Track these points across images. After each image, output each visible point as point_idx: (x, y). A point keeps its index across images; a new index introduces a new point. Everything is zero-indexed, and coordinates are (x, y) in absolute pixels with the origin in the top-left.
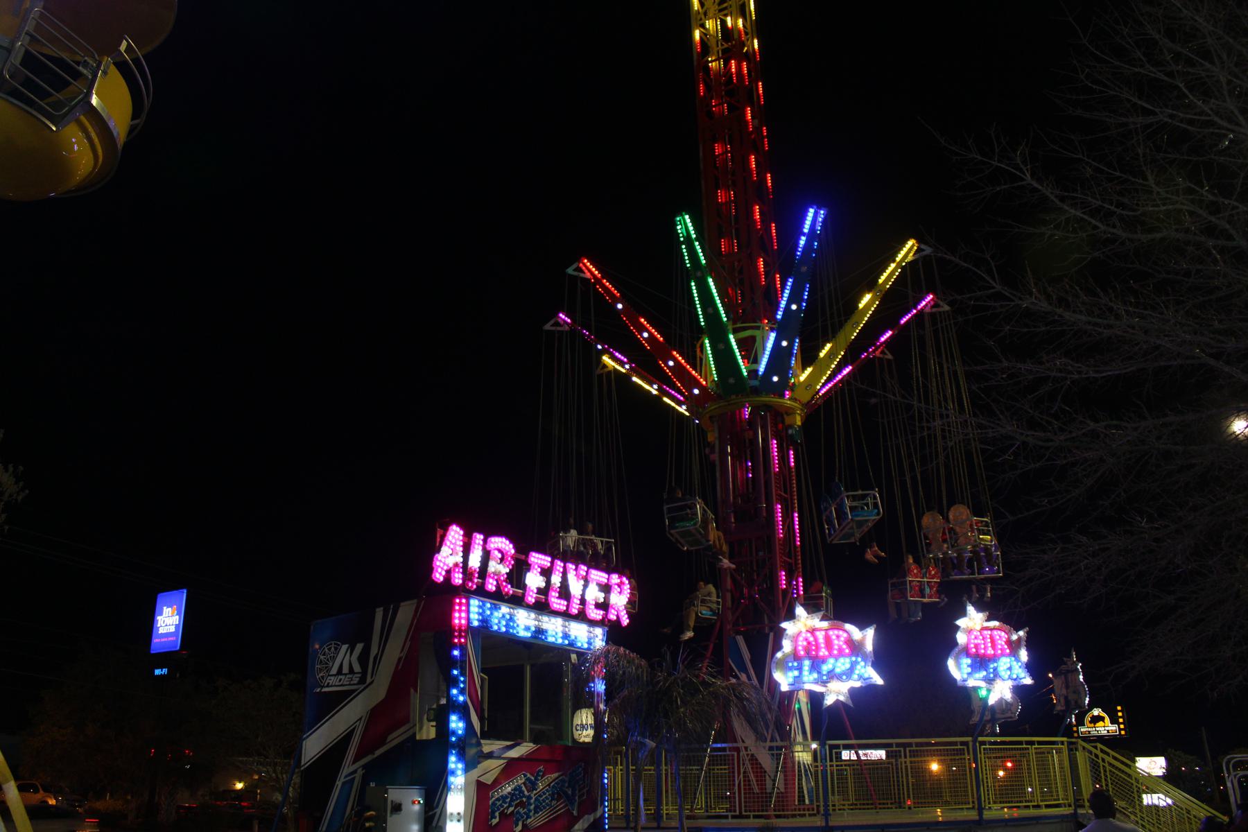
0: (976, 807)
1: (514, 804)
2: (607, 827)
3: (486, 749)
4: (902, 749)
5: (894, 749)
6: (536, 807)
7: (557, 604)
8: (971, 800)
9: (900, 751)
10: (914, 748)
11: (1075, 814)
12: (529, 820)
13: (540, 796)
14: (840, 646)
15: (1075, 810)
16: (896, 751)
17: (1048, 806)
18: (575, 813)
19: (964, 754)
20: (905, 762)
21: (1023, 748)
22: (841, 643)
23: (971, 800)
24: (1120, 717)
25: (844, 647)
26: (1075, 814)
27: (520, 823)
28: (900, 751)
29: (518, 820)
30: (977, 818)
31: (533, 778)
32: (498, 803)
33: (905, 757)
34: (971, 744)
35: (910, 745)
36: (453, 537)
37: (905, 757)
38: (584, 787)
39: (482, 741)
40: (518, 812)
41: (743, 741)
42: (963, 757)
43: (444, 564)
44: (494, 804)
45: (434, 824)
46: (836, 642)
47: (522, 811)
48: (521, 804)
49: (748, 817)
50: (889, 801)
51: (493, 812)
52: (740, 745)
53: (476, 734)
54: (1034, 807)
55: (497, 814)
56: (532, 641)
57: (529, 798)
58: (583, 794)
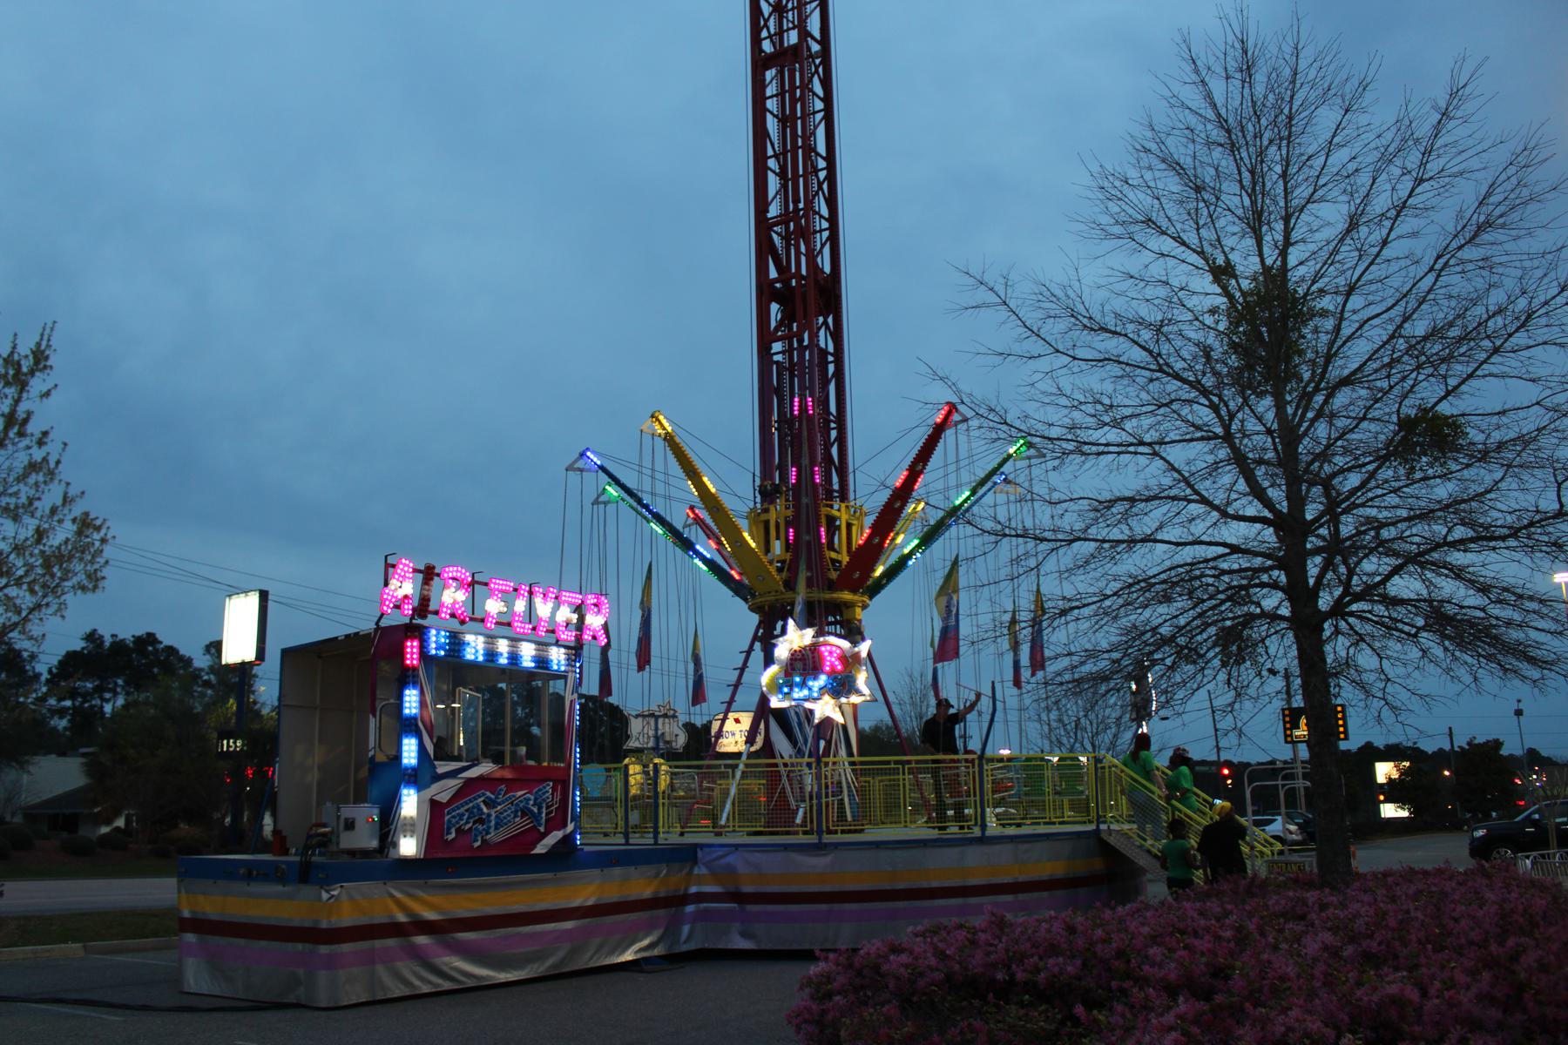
0: (979, 823)
1: (472, 821)
2: (578, 842)
3: (440, 770)
4: (730, 770)
5: (893, 766)
6: (497, 824)
7: (520, 628)
8: (903, 820)
9: (898, 769)
10: (913, 765)
11: (1098, 830)
12: (489, 837)
13: (501, 813)
14: (832, 663)
15: (1098, 826)
16: (894, 769)
17: (843, 832)
18: (542, 829)
19: (898, 774)
20: (904, 779)
21: (890, 769)
22: (829, 658)
23: (903, 820)
24: (1341, 726)
25: (837, 663)
26: (1098, 830)
27: (479, 838)
28: (898, 769)
29: (476, 836)
30: (817, 841)
31: (493, 796)
32: (454, 821)
33: (904, 774)
34: (977, 762)
35: (909, 762)
36: (402, 570)
37: (904, 774)
38: (552, 805)
39: (436, 763)
40: (476, 829)
41: (782, 757)
42: (896, 777)
43: (393, 596)
44: (449, 821)
45: (390, 839)
46: (829, 658)
47: (480, 827)
48: (481, 821)
49: (836, 832)
50: (865, 822)
51: (449, 829)
52: (778, 761)
53: (429, 756)
54: (1045, 823)
55: (453, 830)
56: (509, 667)
57: (489, 815)
58: (551, 812)
